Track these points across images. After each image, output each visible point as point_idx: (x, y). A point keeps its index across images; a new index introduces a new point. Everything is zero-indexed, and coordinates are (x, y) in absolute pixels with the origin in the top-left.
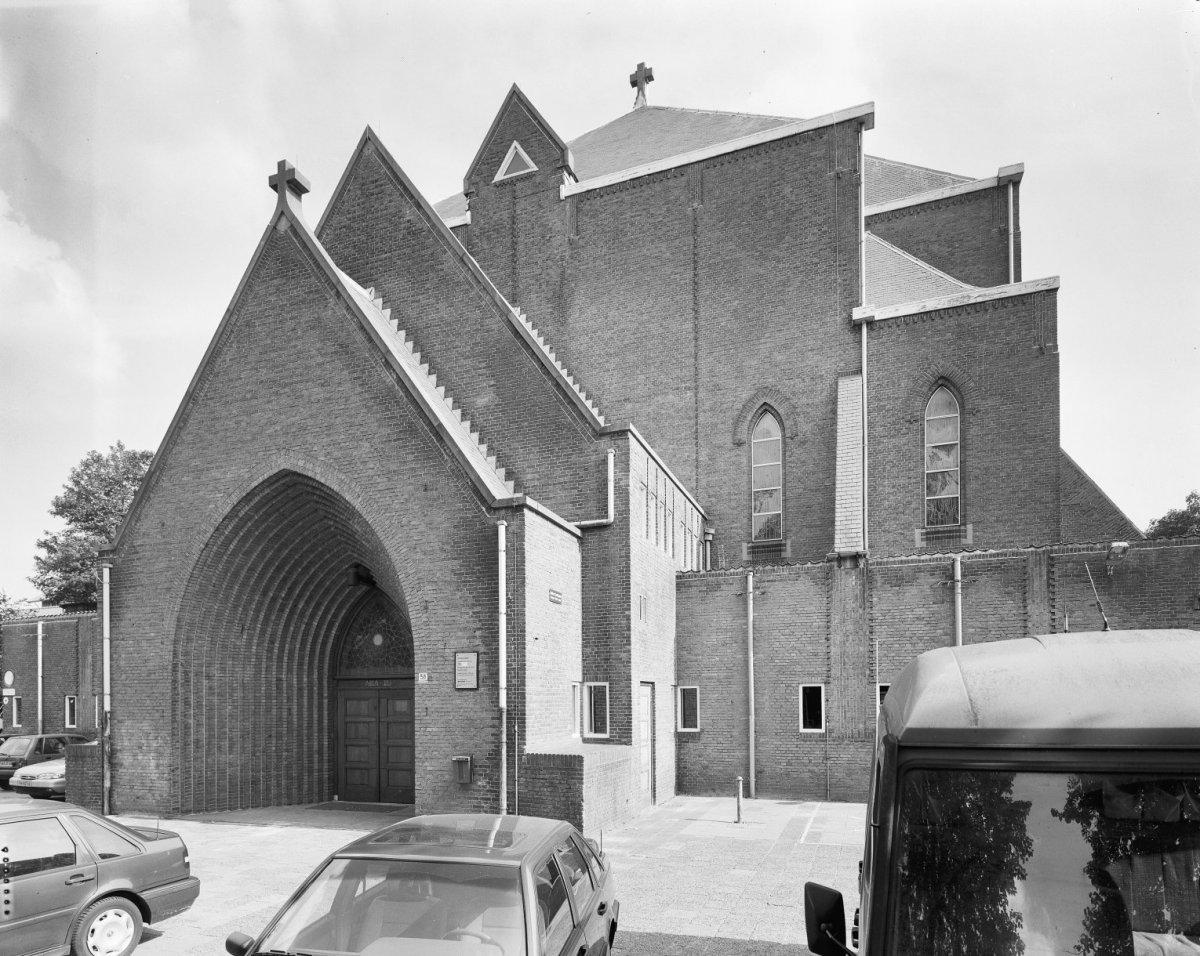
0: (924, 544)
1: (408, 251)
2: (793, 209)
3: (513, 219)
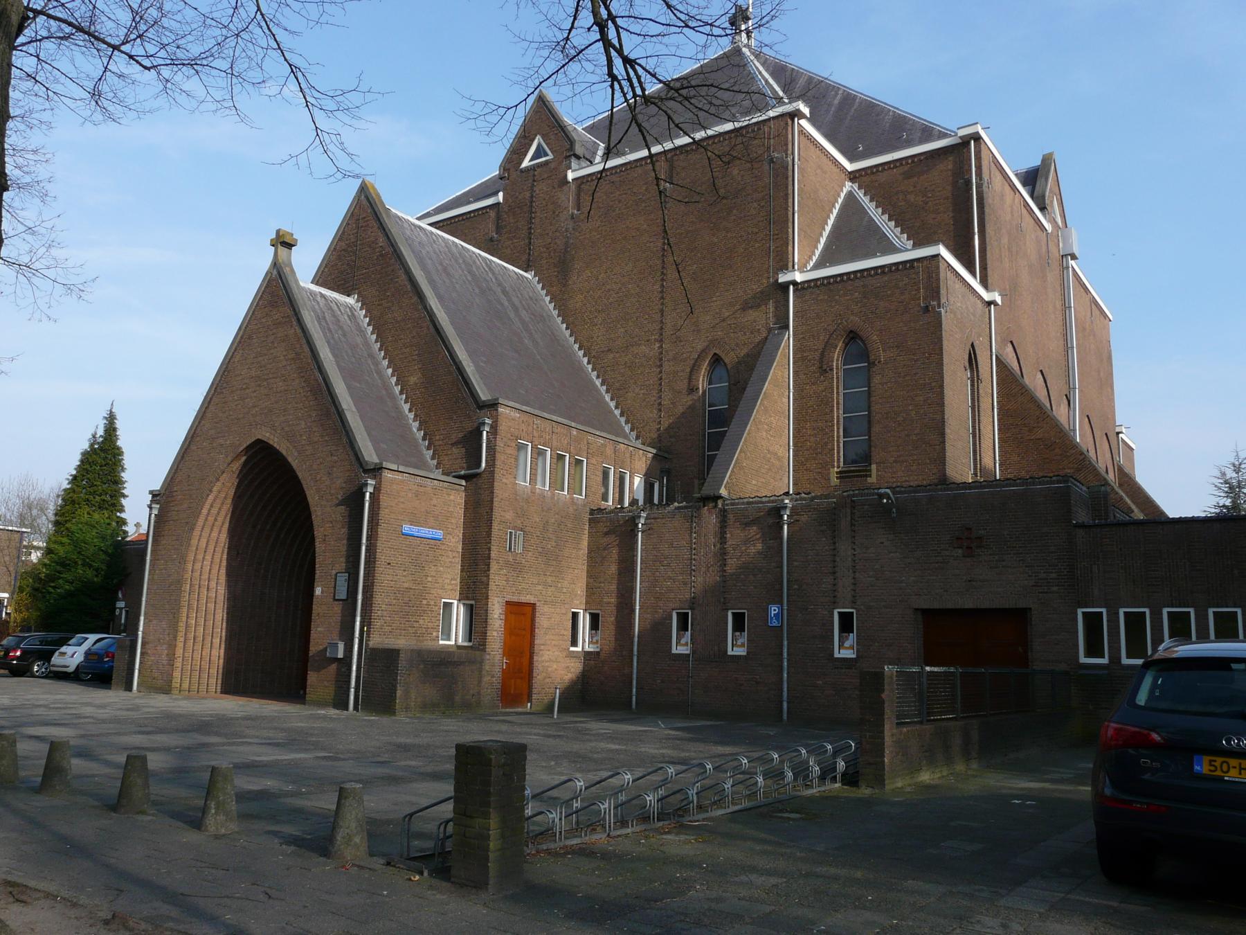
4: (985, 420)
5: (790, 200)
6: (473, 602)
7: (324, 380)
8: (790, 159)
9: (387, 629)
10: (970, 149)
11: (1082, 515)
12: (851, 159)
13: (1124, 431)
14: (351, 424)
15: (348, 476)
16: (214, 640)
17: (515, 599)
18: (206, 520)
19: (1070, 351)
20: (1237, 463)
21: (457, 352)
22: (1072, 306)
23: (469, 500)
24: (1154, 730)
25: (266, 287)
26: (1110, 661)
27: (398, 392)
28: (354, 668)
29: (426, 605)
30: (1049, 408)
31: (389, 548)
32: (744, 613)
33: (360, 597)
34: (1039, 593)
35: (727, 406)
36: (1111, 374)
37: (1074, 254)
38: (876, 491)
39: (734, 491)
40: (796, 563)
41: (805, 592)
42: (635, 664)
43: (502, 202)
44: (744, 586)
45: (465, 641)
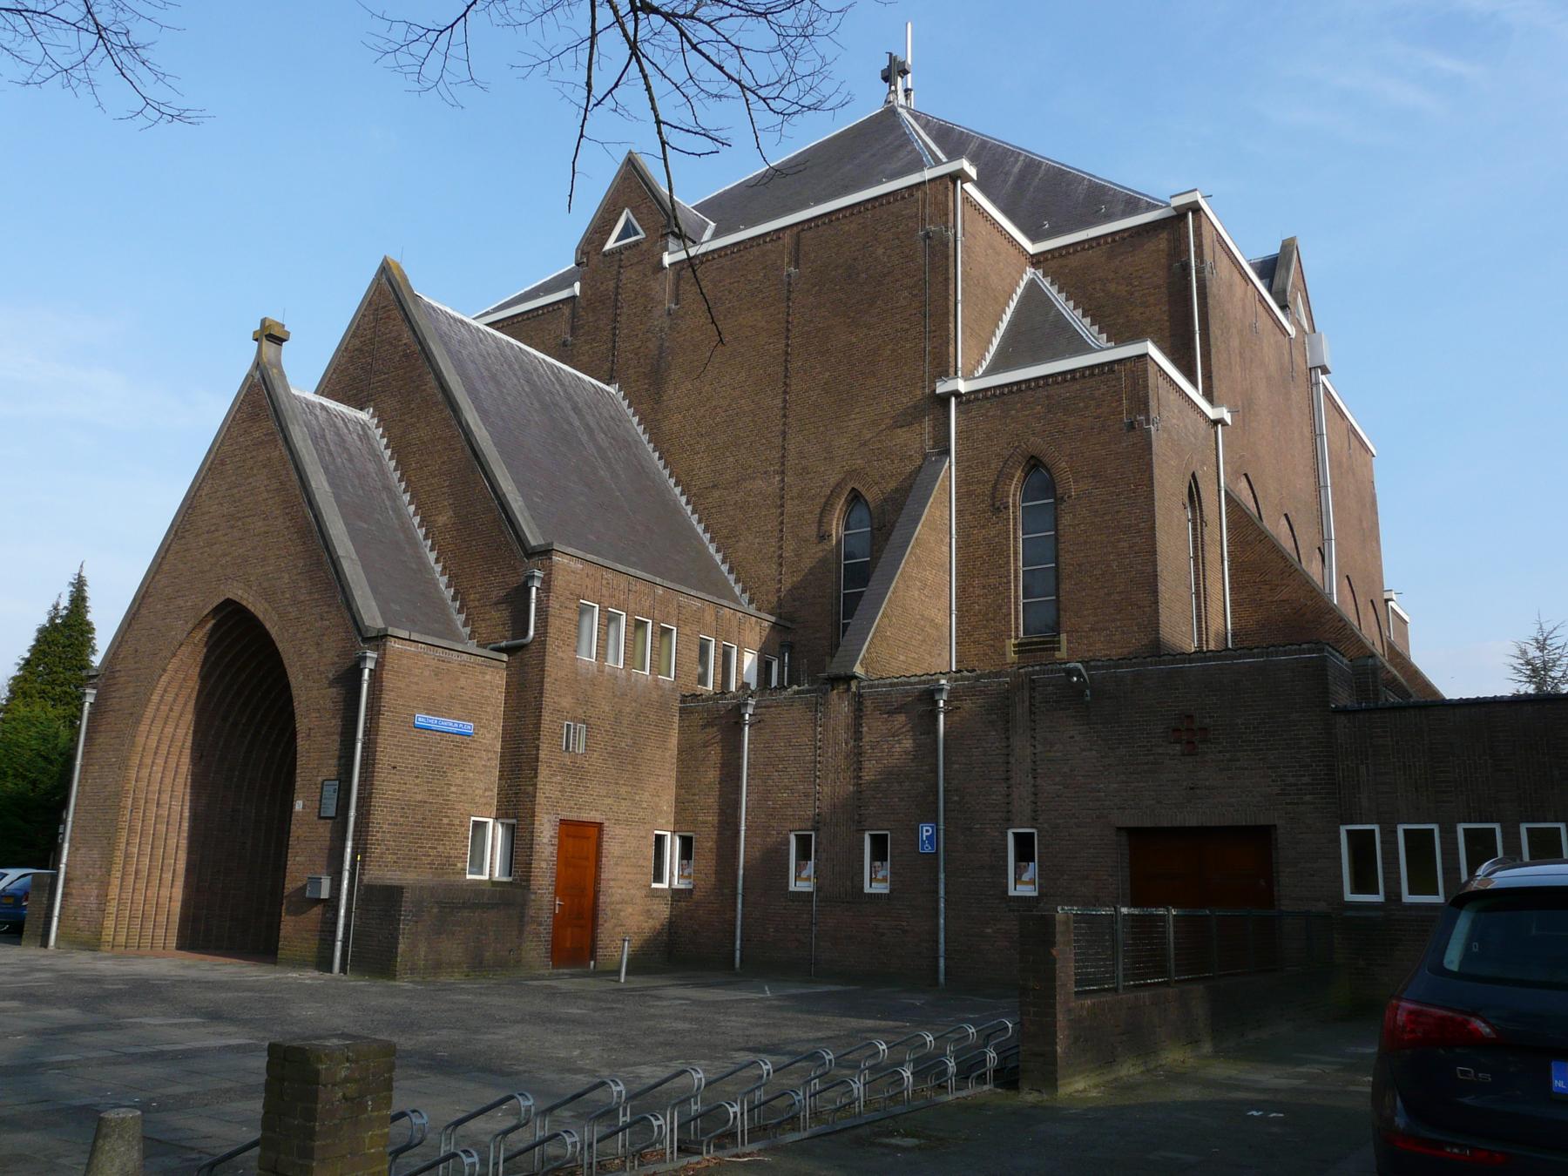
2: (886, 271)
4: (1213, 576)
5: (952, 287)
6: (514, 821)
7: (315, 516)
8: (951, 233)
9: (390, 858)
10: (1187, 223)
11: (1343, 697)
12: (1034, 239)
13: (1394, 598)
14: (349, 578)
15: (344, 647)
16: (164, 876)
17: (573, 816)
18: (158, 709)
19: (1322, 492)
20: (1541, 638)
21: (500, 482)
22: (1325, 432)
23: (512, 682)
24: (1475, 1014)
25: (246, 395)
26: (1386, 899)
27: (421, 537)
28: (342, 912)
29: (448, 824)
30: (1297, 559)
31: (394, 745)
32: (887, 835)
33: (352, 813)
34: (1287, 803)
35: (868, 559)
36: (1377, 524)
37: (1325, 366)
38: (1063, 666)
39: (873, 668)
40: (956, 766)
42: (740, 906)
43: (578, 294)
44: (886, 798)
45: (504, 875)
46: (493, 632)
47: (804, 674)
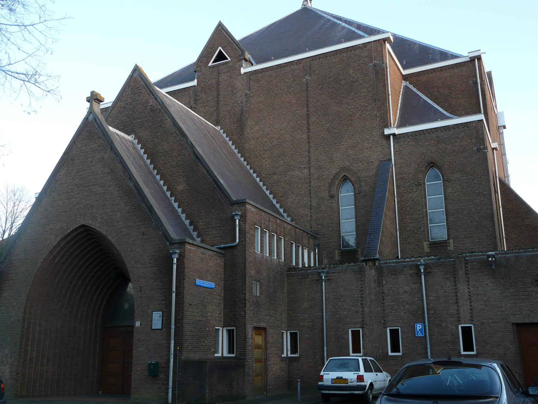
0: (429, 250)
1: (150, 118)
3: (218, 83)
33: (173, 326)
41: (438, 315)
46: (215, 240)
47: (325, 258)
